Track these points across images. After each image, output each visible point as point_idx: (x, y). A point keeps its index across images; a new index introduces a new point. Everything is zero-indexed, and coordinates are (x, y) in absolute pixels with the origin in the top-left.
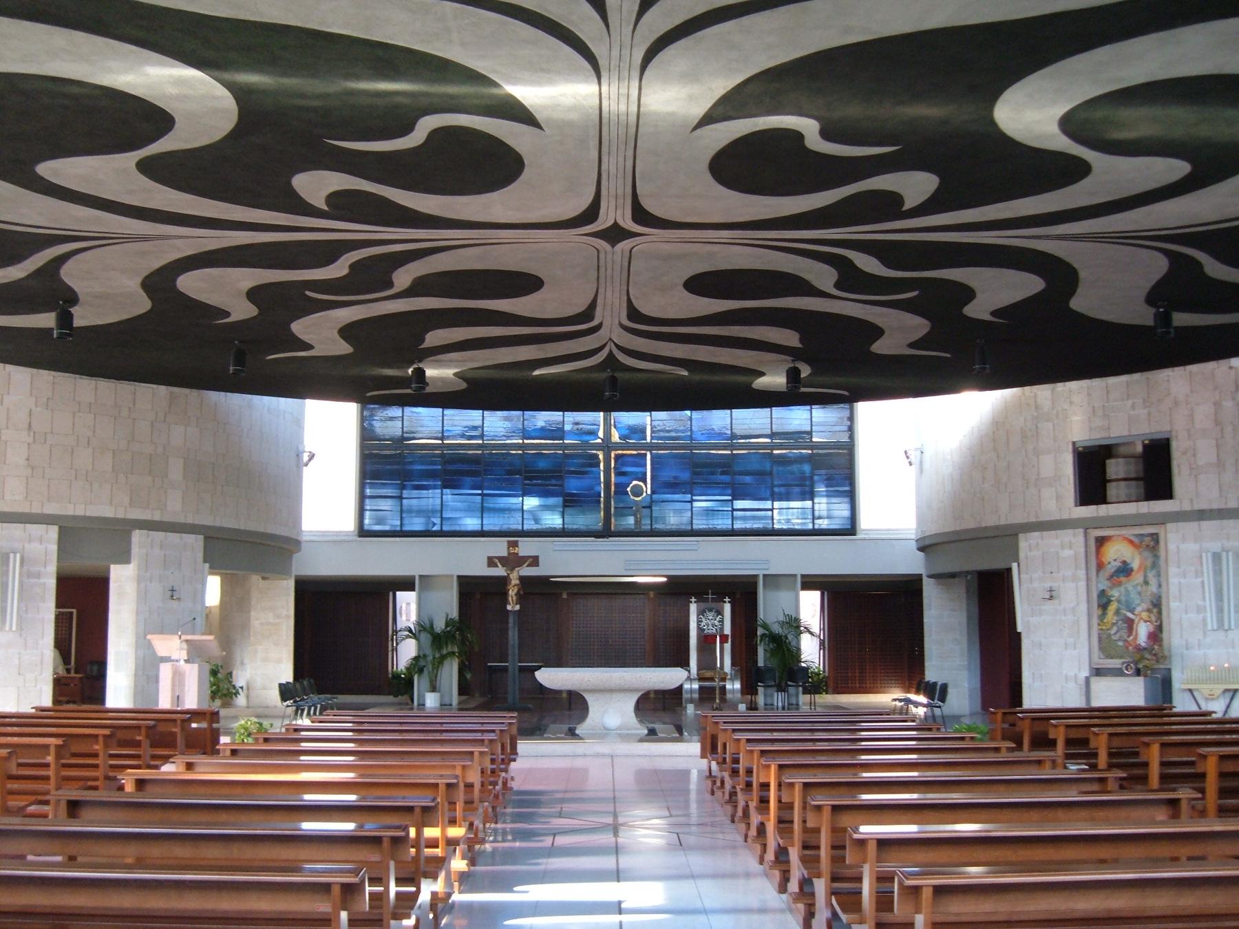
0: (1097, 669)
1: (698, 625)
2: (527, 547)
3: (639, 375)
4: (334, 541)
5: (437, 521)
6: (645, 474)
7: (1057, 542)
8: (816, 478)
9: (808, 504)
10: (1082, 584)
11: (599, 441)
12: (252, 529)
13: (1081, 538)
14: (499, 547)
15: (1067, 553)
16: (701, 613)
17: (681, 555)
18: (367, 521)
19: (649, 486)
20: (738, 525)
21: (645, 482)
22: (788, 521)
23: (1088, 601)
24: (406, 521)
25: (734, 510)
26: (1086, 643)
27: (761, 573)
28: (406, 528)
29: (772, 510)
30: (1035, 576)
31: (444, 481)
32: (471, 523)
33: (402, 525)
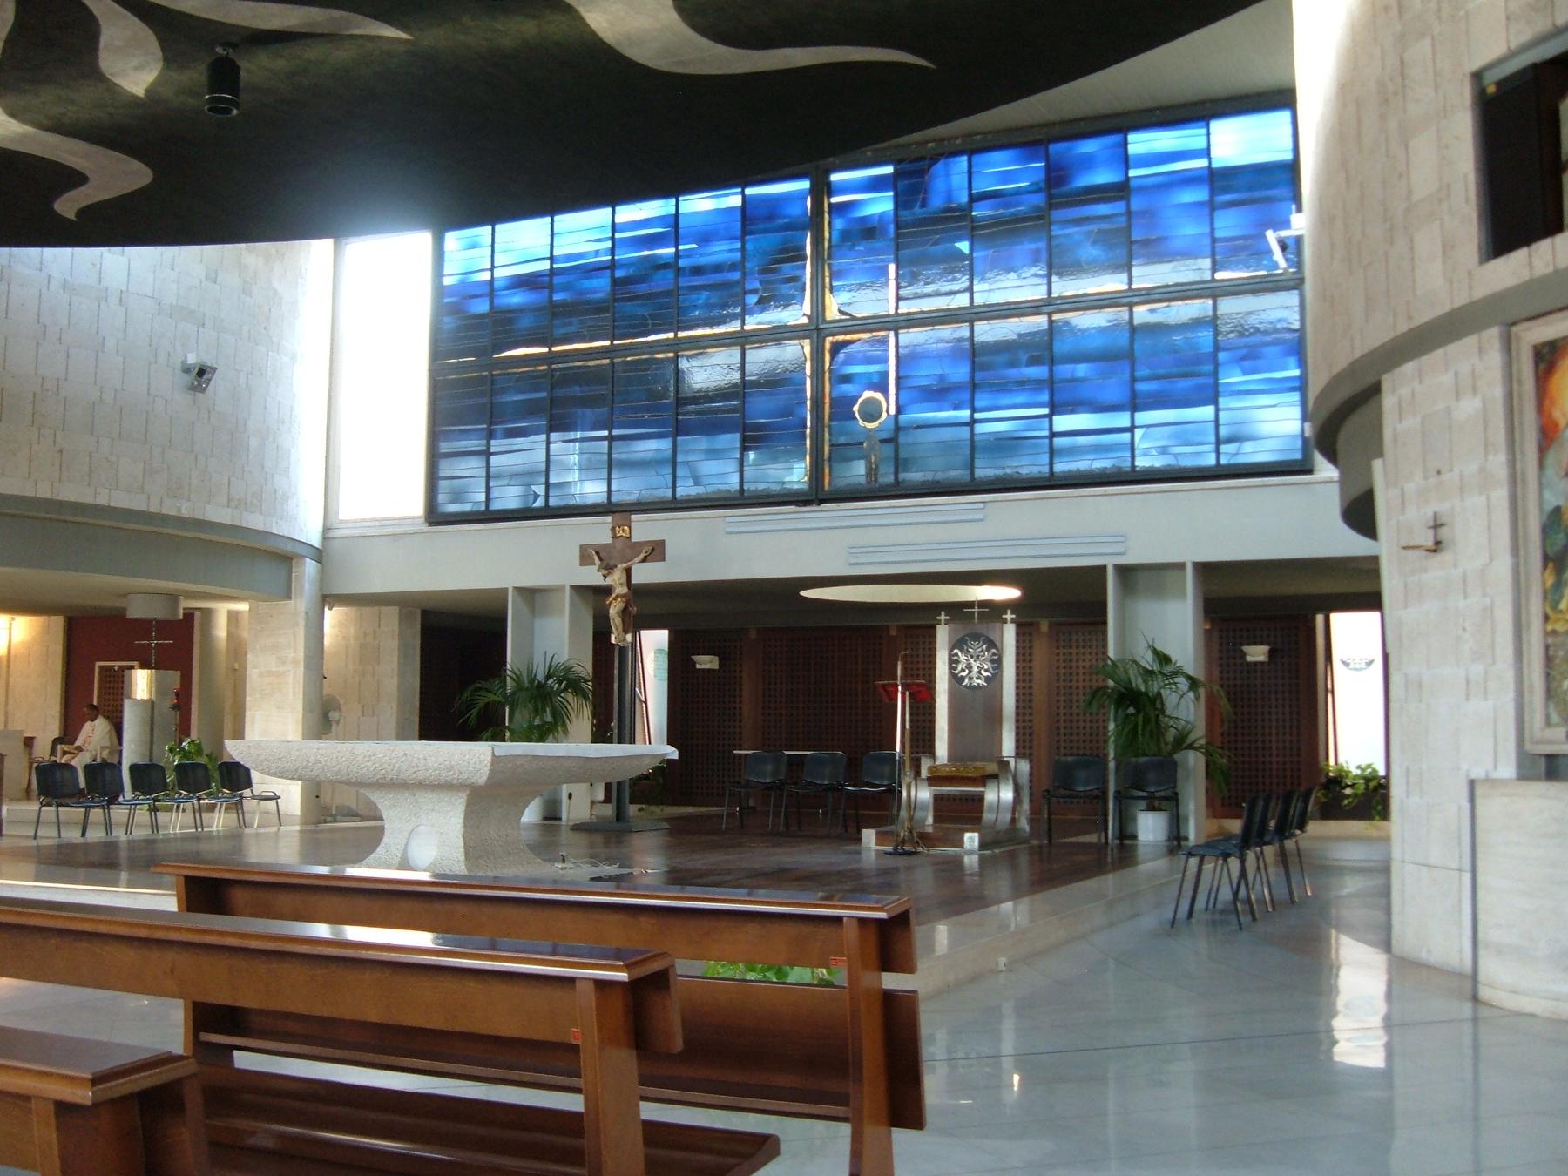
0: (1551, 758)
1: (951, 668)
2: (644, 528)
3: (313, 52)
4: (394, 535)
5: (541, 490)
6: (885, 374)
7: (1447, 379)
8: (1222, 356)
9: (1207, 412)
10: (1501, 495)
13: (1495, 358)
14: (599, 531)
15: (1469, 407)
16: (958, 644)
17: (939, 533)
18: (441, 498)
20: (1061, 467)
21: (885, 392)
22: (1163, 451)
23: (1515, 549)
24: (495, 494)
25: (1053, 435)
26: (1509, 676)
27: (1109, 562)
28: (496, 506)
29: (1131, 429)
30: (1410, 487)
31: (551, 418)
32: (592, 490)
33: (488, 499)
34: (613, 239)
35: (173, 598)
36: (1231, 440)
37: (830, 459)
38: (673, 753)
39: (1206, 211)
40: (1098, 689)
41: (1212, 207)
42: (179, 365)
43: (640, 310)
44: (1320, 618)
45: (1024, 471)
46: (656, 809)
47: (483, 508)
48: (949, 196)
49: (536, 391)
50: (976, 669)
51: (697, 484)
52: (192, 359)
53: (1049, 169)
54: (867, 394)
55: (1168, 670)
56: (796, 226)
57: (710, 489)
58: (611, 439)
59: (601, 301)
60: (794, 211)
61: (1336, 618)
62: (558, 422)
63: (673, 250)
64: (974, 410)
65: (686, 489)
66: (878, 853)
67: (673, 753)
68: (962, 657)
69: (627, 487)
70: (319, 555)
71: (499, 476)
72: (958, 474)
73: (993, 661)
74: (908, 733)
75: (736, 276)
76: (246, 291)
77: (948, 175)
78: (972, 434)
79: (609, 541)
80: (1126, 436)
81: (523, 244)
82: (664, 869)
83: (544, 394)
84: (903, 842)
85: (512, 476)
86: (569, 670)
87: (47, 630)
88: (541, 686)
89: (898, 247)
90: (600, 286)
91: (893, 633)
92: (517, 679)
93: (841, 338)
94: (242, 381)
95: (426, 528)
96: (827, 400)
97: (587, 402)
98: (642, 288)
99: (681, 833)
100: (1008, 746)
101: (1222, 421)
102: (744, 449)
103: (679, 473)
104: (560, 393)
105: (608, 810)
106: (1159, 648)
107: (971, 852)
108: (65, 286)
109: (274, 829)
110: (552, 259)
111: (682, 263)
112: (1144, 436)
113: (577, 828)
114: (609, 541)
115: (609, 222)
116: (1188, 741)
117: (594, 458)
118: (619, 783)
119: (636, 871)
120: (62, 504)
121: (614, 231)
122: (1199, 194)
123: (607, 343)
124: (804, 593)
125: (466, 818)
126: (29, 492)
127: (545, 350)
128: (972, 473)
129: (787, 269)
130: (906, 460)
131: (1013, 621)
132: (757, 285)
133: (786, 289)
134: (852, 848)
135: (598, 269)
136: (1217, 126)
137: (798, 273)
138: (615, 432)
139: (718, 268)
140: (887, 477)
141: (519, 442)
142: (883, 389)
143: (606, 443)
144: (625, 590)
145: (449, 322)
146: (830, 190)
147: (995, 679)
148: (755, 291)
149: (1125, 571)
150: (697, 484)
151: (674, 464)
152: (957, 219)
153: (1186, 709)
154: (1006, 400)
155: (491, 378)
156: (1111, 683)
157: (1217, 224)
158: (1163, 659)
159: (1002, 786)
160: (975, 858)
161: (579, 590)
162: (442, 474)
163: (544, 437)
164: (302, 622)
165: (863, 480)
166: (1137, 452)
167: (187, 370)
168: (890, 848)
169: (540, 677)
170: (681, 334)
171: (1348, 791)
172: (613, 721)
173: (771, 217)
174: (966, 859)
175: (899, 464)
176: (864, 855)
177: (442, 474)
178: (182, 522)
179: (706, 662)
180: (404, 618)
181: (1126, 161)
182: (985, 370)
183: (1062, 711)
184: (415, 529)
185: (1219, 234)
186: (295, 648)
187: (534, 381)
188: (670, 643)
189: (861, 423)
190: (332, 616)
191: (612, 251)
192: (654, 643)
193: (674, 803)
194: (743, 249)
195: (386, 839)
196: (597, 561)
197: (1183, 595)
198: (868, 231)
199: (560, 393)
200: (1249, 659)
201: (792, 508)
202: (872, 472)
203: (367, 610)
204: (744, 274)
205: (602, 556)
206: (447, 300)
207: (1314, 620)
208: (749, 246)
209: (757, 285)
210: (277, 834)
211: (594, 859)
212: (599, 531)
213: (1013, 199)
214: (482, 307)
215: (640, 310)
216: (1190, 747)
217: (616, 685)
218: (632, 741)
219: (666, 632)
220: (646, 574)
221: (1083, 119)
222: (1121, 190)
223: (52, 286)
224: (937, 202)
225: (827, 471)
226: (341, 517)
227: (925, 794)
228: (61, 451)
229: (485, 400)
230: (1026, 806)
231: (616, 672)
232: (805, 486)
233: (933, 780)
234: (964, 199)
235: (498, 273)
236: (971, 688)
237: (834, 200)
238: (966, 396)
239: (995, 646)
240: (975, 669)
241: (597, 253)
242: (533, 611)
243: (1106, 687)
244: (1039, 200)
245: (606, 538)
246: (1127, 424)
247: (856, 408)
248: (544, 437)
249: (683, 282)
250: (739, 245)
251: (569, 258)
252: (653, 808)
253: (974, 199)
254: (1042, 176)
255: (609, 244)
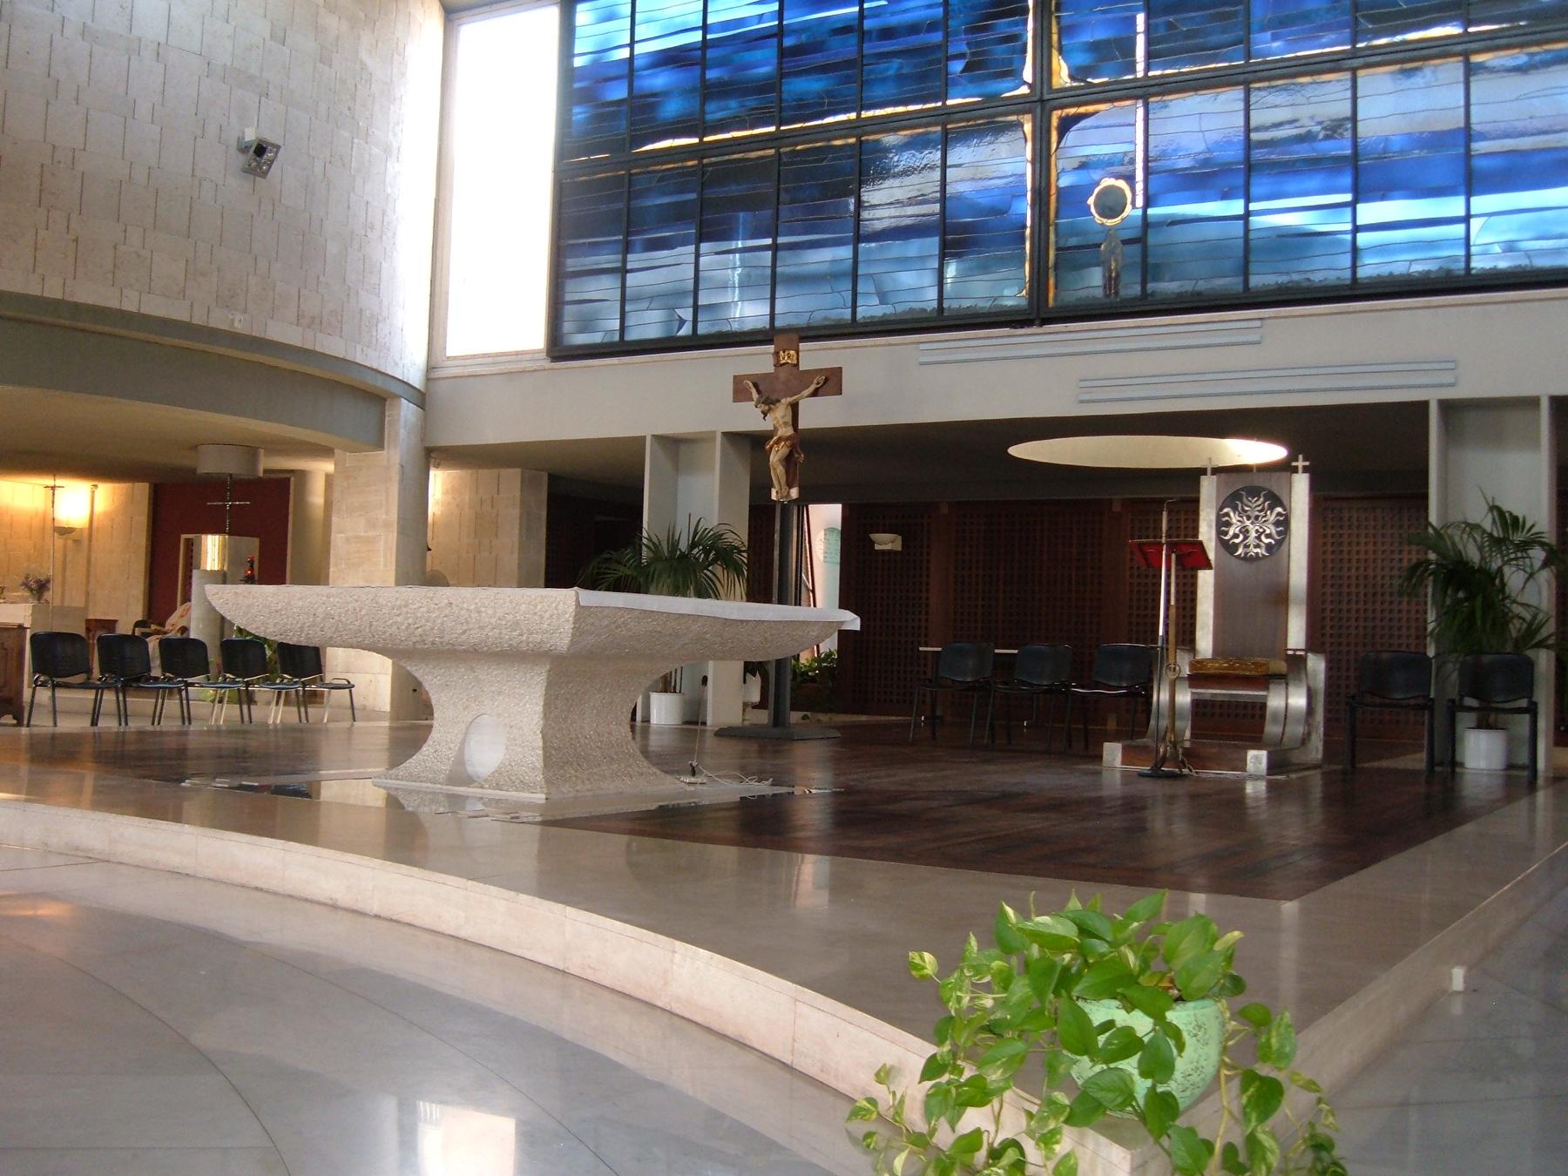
1: (1220, 533)
2: (814, 356)
5: (687, 314)
11: (1024, 90)
12: (160, 312)
18: (567, 326)
19: (1140, 187)
21: (1130, 179)
22: (1510, 247)
27: (1433, 397)
28: (633, 335)
29: (1466, 219)
32: (749, 313)
35: (251, 451)
38: (852, 621)
40: (1418, 565)
42: (233, 143)
45: (1317, 277)
46: (824, 717)
47: (617, 338)
49: (682, 192)
50: (1251, 530)
52: (250, 136)
55: (1518, 537)
57: (900, 308)
58: (775, 248)
62: (711, 229)
63: (856, 9)
64: (1248, 201)
65: (870, 308)
66: (1125, 774)
67: (852, 621)
68: (1234, 518)
69: (794, 307)
70: (421, 399)
71: (638, 299)
72: (1229, 283)
73: (1277, 524)
74: (1173, 611)
75: (937, 37)
76: (324, 58)
78: (1247, 229)
79: (771, 369)
80: (1460, 229)
83: (693, 196)
84: (1164, 761)
86: (719, 537)
87: (131, 499)
88: (683, 556)
90: (763, 63)
91: (1117, 508)
93: (1072, 111)
94: (318, 166)
95: (548, 364)
97: (749, 203)
98: (818, 59)
99: (852, 745)
100: (1296, 634)
102: (943, 257)
103: (860, 289)
104: (710, 193)
105: (763, 717)
106: (1505, 507)
107: (1256, 778)
108: (84, 32)
109: (347, 724)
110: (705, 28)
111: (868, 24)
112: (1483, 228)
113: (724, 733)
114: (771, 369)
116: (1538, 638)
117: (754, 272)
118: (779, 662)
119: (798, 791)
120: (77, 309)
123: (773, 129)
124: (1016, 451)
125: (547, 705)
126: (34, 289)
127: (696, 140)
128: (1246, 281)
129: (1003, 26)
130: (1157, 266)
131: (1305, 470)
132: (964, 48)
133: (1000, 51)
135: (760, 38)
137: (1015, 30)
138: (781, 240)
139: (914, 29)
143: (770, 253)
144: (789, 431)
145: (580, 113)
149: (1450, 408)
151: (855, 277)
153: (1532, 590)
154: (1292, 186)
156: (1432, 556)
158: (1510, 522)
159: (1291, 689)
160: (1262, 786)
161: (732, 437)
162: (568, 297)
163: (692, 248)
164: (396, 477)
165: (1099, 293)
166: (1473, 250)
167: (243, 149)
168: (1146, 769)
169: (683, 546)
170: (865, 114)
174: (1250, 788)
175: (1148, 271)
176: (1105, 774)
177: (568, 297)
178: (235, 339)
179: (886, 542)
180: (527, 484)
183: (1329, 607)
184: (536, 365)
186: (387, 507)
187: (680, 180)
188: (844, 518)
189: (1098, 219)
190: (440, 482)
192: (825, 518)
193: (845, 712)
196: (755, 395)
197: (1535, 444)
199: (710, 193)
201: (1006, 331)
202: (1111, 282)
204: (947, 35)
205: (763, 391)
206: (577, 85)
209: (964, 48)
210: (350, 730)
211: (745, 772)
212: (759, 360)
214: (619, 92)
217: (776, 553)
218: (798, 603)
220: (819, 414)
223: (68, 32)
225: (1052, 281)
226: (449, 353)
227: (1184, 698)
228: (76, 240)
229: (621, 205)
230: (1320, 716)
231: (777, 537)
232: (1024, 303)
235: (640, 49)
239: (1281, 504)
240: (1253, 534)
241: (760, 18)
243: (1429, 562)
246: (1460, 211)
247: (1091, 201)
248: (692, 248)
249: (869, 48)
251: (726, 25)
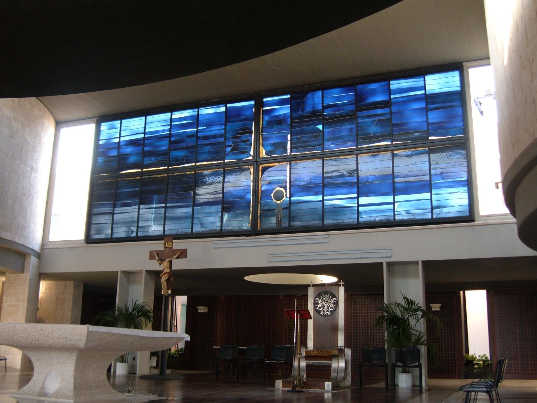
1: (315, 307)
2: (178, 245)
4: (69, 247)
5: (134, 229)
9: (427, 195)
14: (159, 246)
18: (92, 232)
22: (407, 212)
24: (115, 231)
27: (384, 261)
28: (115, 236)
29: (394, 203)
31: (140, 199)
32: (156, 229)
34: (171, 125)
36: (438, 207)
37: (260, 216)
39: (424, 112)
40: (380, 318)
41: (426, 110)
43: (180, 154)
44: (462, 292)
45: (346, 221)
46: (179, 372)
47: (110, 237)
48: (314, 105)
50: (326, 306)
51: (202, 227)
53: (356, 95)
54: (279, 189)
55: (413, 308)
56: (249, 119)
57: (208, 229)
58: (166, 207)
59: (164, 150)
60: (248, 113)
61: (467, 292)
62: (144, 199)
65: (198, 229)
66: (283, 391)
68: (320, 302)
69: (172, 228)
70: (39, 256)
71: (118, 223)
72: (318, 223)
73: (334, 304)
74: (299, 334)
75: (222, 140)
77: (313, 98)
79: (163, 249)
80: (391, 206)
81: (133, 127)
82: (181, 397)
83: (139, 189)
84: (296, 386)
85: (123, 223)
86: (143, 307)
89: (292, 127)
90: (164, 146)
91: (281, 298)
92: (120, 311)
93: (266, 165)
95: (85, 245)
96: (260, 191)
97: (158, 192)
99: (189, 382)
101: (433, 200)
103: (194, 222)
104: (145, 188)
105: (156, 372)
107: (328, 392)
110: (145, 133)
111: (199, 134)
113: (143, 377)
114: (163, 249)
115: (170, 118)
117: (158, 215)
121: (171, 122)
122: (422, 105)
124: (247, 278)
127: (140, 170)
128: (323, 222)
129: (244, 137)
130: (294, 217)
131: (343, 285)
133: (243, 145)
134: (273, 389)
136: (428, 77)
137: (248, 138)
138: (168, 205)
139: (214, 137)
140: (285, 224)
141: (127, 209)
142: (285, 188)
143: (164, 209)
144: (169, 270)
145: (100, 160)
146: (264, 105)
147: (335, 311)
148: (230, 146)
149: (389, 264)
150: (202, 227)
151: (193, 218)
152: (317, 116)
153: (418, 325)
154: (338, 191)
155: (116, 183)
156: (386, 314)
157: (429, 117)
158: (410, 303)
160: (330, 395)
162: (93, 222)
163: (137, 207)
164: (28, 283)
165: (275, 225)
168: (290, 389)
170: (197, 164)
171: (476, 366)
172: (160, 319)
173: (238, 115)
174: (326, 395)
175: (291, 218)
176: (276, 392)
179: (202, 309)
180: (76, 287)
181: (390, 92)
182: (324, 185)
184: (80, 245)
185: (430, 121)
186: (24, 294)
187: (134, 183)
188: (188, 301)
190: (43, 286)
191: (170, 130)
194: (225, 129)
195: (34, 378)
196: (157, 258)
197: (418, 276)
198: (279, 121)
199: (145, 188)
200: (433, 309)
202: (279, 222)
203: (61, 283)
204: (225, 139)
205: (160, 256)
206: (100, 150)
207: (460, 293)
208: (228, 128)
209: (231, 144)
211: (151, 392)
212: (159, 246)
213: (342, 107)
214: (114, 153)
215: (180, 154)
216: (422, 344)
219: (186, 297)
220: (179, 265)
221: (371, 75)
222: (387, 104)
224: (308, 109)
225: (259, 221)
227: (303, 364)
232: (250, 228)
233: (307, 357)
234: (320, 107)
236: (324, 315)
237: (264, 109)
238: (321, 189)
241: (164, 131)
242: (129, 281)
243: (384, 316)
244: (352, 108)
245: (161, 248)
247: (272, 195)
248: (137, 207)
249: (200, 142)
250: (224, 127)
252: (178, 371)
253: (324, 107)
254: (354, 98)
255: (169, 127)
